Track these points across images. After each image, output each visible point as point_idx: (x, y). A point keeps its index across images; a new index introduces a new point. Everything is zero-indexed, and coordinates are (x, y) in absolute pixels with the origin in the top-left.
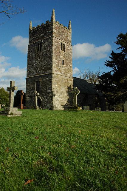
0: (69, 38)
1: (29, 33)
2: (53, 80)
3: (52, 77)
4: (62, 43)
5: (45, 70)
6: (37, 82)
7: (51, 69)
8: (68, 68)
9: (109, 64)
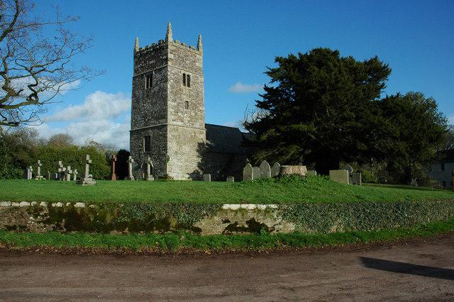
0: (197, 64)
1: (135, 57)
2: (169, 135)
3: (166, 131)
4: (184, 75)
5: (157, 119)
6: (146, 137)
7: (165, 117)
8: (196, 114)
9: (261, 105)
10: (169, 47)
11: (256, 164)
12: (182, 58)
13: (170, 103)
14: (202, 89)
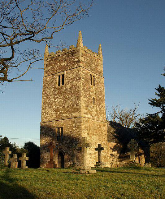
0: (99, 68)
8: (100, 109)
10: (81, 51)
11: (118, 153)
12: (89, 61)
13: (83, 99)
14: (103, 89)
